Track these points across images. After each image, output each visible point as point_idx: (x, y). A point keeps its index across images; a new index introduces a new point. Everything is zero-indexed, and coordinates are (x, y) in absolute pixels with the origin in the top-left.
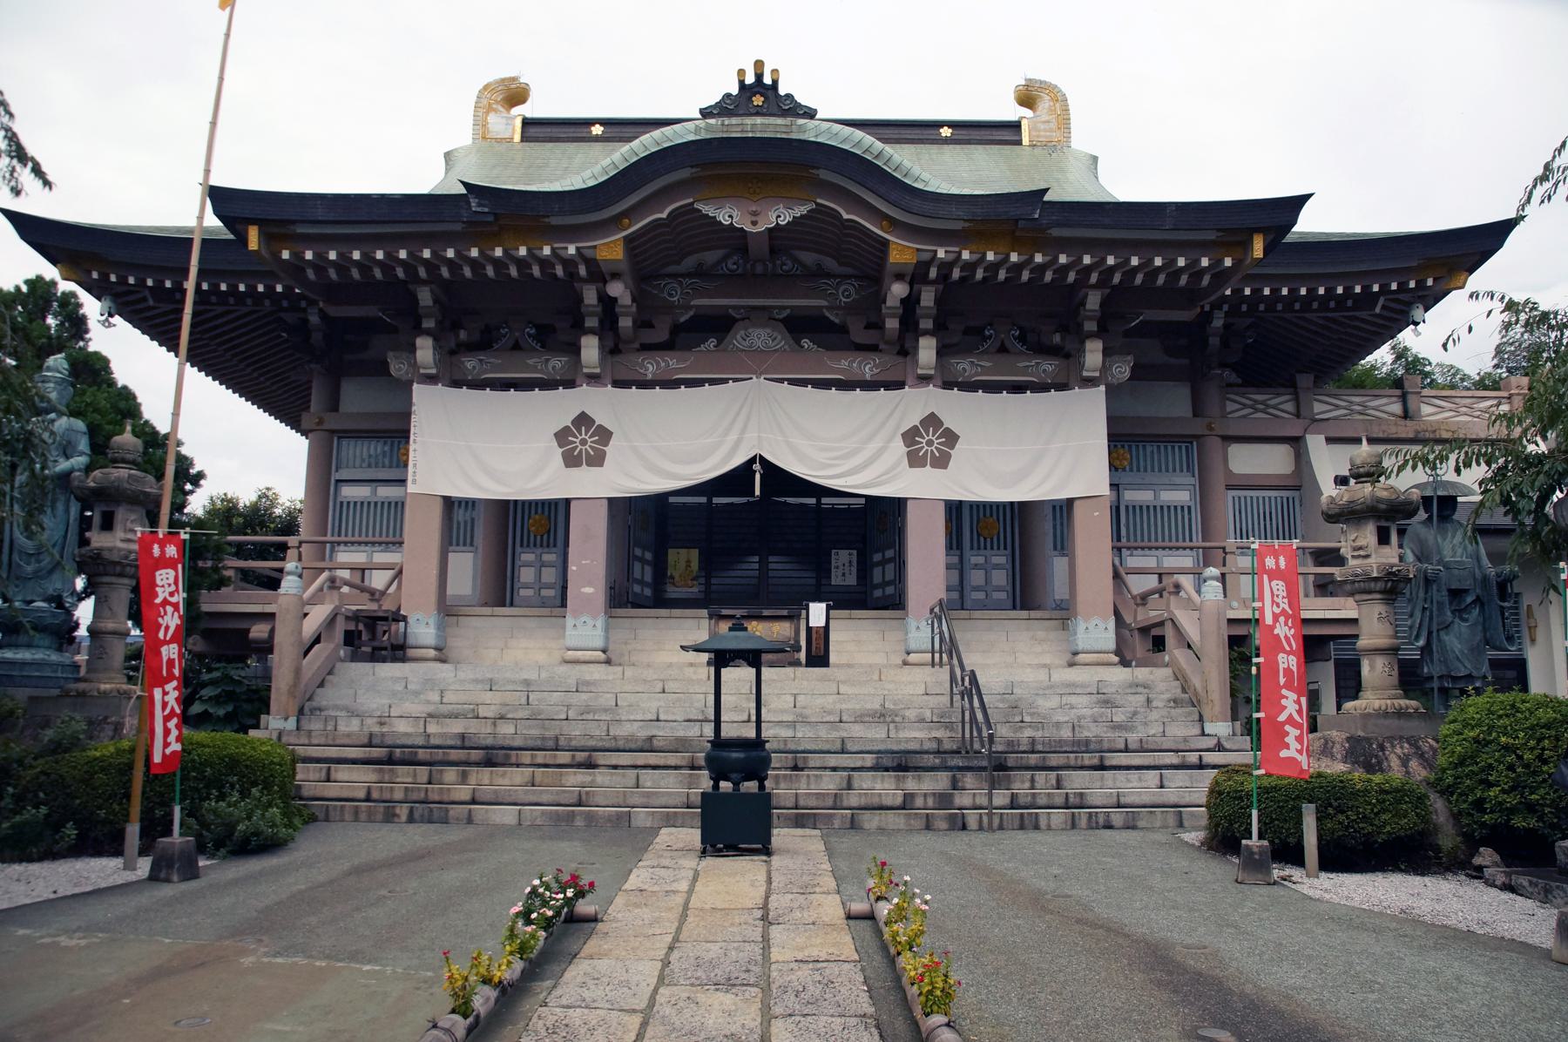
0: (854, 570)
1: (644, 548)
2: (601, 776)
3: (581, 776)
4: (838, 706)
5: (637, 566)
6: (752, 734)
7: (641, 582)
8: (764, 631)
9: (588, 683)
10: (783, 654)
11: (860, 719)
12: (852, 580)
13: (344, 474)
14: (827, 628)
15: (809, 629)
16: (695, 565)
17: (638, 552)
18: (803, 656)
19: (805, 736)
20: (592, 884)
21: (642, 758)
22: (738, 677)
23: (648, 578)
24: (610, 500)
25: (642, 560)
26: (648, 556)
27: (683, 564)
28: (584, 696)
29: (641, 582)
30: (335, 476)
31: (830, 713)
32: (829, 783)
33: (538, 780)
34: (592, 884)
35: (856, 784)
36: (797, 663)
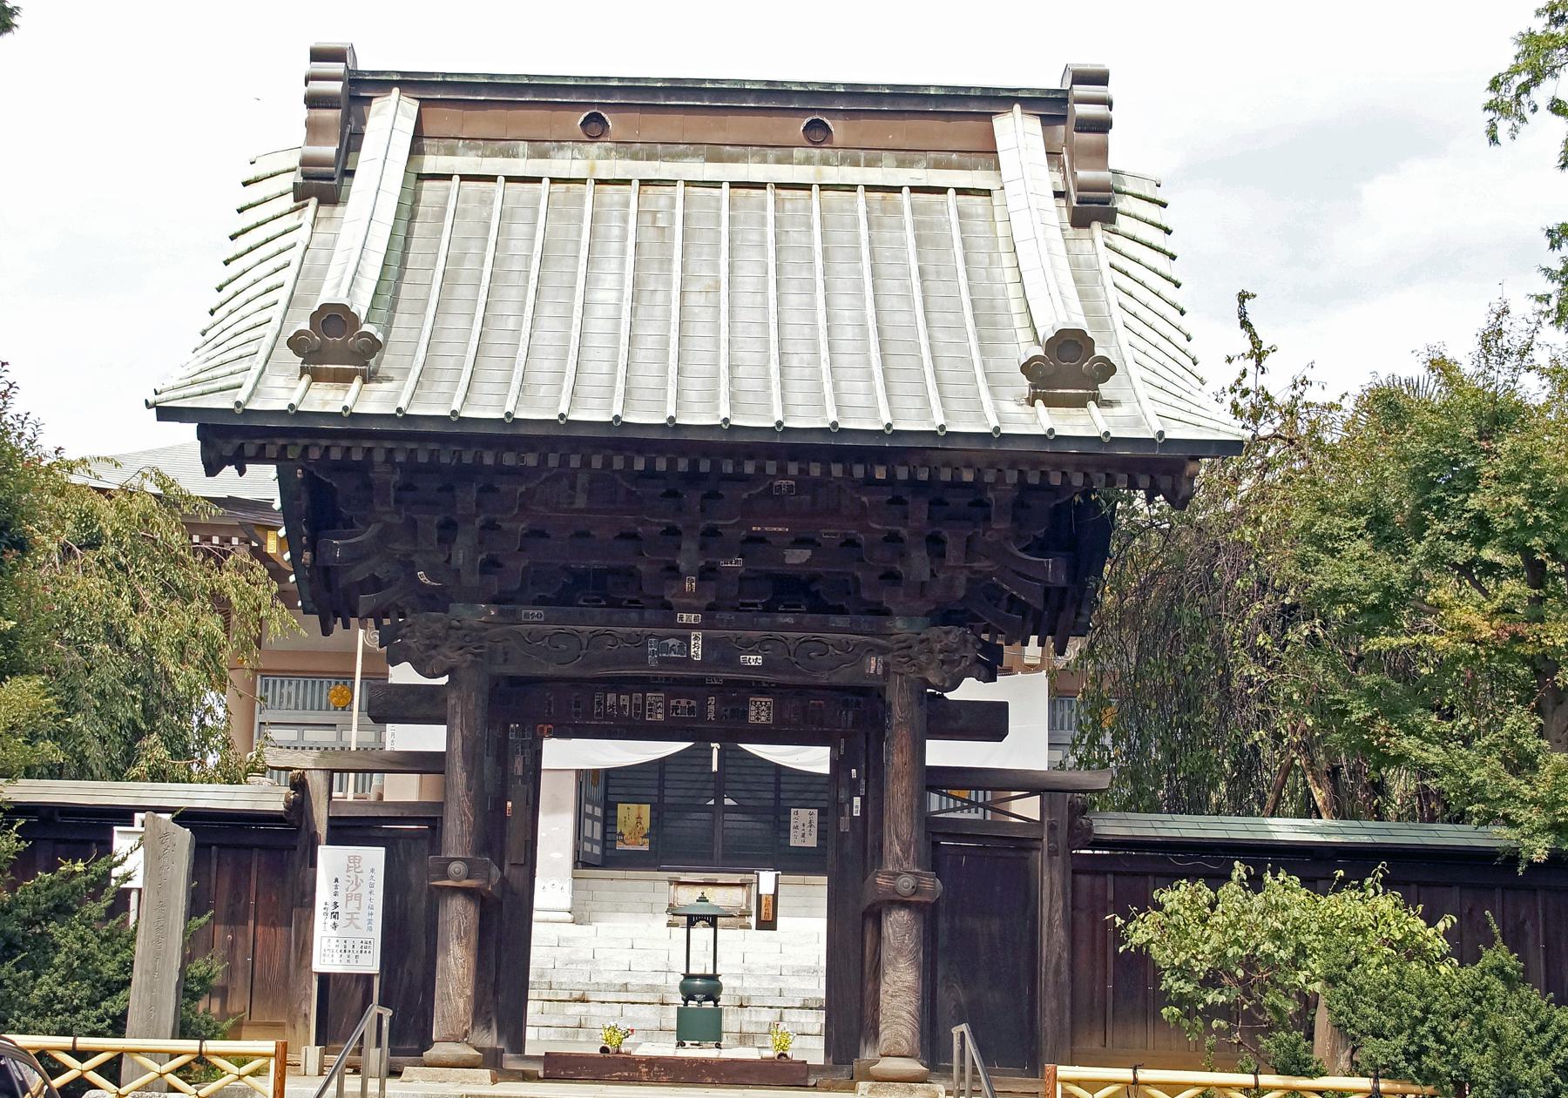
0: (814, 830)
1: (594, 804)
2: (594, 1009)
3: (579, 1008)
4: (780, 963)
5: (588, 822)
6: (710, 971)
7: (592, 840)
8: (720, 898)
9: (567, 940)
10: (738, 917)
11: (797, 972)
12: (812, 841)
13: (268, 716)
14: (775, 896)
15: (759, 897)
16: (646, 823)
17: (589, 809)
18: (753, 921)
19: (750, 986)
20: (1538, 14)
21: (623, 997)
22: (702, 934)
23: (598, 836)
24: (579, 772)
25: (592, 817)
26: (598, 812)
27: (633, 821)
28: (566, 950)
29: (592, 840)
30: (258, 719)
31: (773, 968)
32: (768, 1016)
33: (546, 1010)
34: (1538, 14)
35: (786, 1018)
36: (748, 927)
